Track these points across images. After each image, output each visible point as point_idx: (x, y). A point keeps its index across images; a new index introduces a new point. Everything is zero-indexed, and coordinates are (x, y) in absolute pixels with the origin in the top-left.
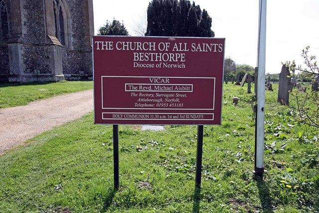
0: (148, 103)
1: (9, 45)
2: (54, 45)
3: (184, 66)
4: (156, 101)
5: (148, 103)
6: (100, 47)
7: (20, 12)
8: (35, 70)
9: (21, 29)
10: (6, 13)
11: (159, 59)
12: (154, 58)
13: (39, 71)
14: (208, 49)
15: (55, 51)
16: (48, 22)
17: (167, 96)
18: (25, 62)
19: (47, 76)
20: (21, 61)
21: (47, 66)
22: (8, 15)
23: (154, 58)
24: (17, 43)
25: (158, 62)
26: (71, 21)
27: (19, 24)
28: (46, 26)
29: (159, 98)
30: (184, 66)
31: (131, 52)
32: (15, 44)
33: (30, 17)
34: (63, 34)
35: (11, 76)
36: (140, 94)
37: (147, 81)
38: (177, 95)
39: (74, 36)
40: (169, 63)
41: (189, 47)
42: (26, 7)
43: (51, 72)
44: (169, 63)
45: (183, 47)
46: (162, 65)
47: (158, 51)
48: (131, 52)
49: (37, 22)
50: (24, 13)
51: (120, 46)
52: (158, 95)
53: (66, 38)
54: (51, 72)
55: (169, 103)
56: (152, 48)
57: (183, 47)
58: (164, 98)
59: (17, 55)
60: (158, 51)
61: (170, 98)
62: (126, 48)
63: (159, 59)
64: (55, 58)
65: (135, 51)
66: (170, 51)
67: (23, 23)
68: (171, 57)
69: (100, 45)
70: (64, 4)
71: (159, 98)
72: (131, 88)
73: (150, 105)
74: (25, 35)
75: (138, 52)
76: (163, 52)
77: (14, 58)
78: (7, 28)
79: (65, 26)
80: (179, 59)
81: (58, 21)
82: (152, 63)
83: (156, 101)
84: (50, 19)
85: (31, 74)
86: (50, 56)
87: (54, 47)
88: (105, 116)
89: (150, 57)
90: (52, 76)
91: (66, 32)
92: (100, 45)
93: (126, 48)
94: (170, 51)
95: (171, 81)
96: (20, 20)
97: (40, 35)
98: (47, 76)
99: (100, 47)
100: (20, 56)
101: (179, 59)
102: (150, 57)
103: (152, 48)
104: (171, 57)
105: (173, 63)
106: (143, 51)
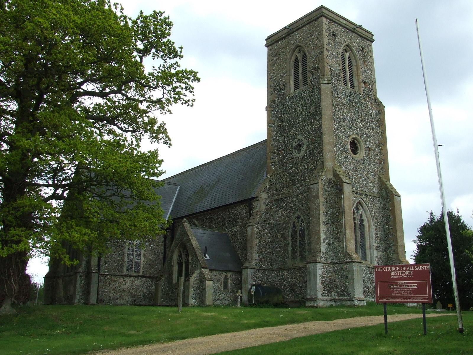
0: (398, 293)
1: (308, 265)
2: (354, 262)
3: (412, 276)
4: (401, 292)
5: (398, 293)
6: (377, 270)
7: (320, 230)
8: (333, 293)
9: (320, 247)
10: (304, 229)
11: (401, 274)
12: (399, 274)
13: (336, 294)
14: (422, 269)
15: (354, 268)
16: (347, 236)
17: (406, 290)
18: (323, 283)
19: (345, 300)
20: (319, 283)
21: (345, 288)
22: (307, 232)
23: (399, 274)
24: (316, 262)
25: (401, 275)
26: (373, 230)
27: (318, 242)
28: (346, 241)
29: (403, 291)
30: (412, 276)
31: (389, 272)
32: (314, 264)
33: (329, 234)
34: (363, 247)
35: (308, 300)
36: (394, 289)
37: (397, 283)
38: (411, 289)
39: (377, 248)
40: (406, 275)
41: (414, 268)
42: (325, 224)
43: (349, 295)
44: (406, 275)
45: (411, 269)
46: (403, 276)
47: (400, 270)
48: (389, 272)
49: (337, 237)
50: (323, 229)
51: (385, 269)
52: (402, 290)
53: (368, 252)
54: (349, 295)
55: (407, 293)
56: (398, 269)
57: (411, 269)
58: (405, 291)
59: (315, 275)
60: (400, 270)
61: (408, 291)
62: (387, 270)
63: (401, 274)
64: (355, 278)
65: (391, 271)
66: (406, 270)
67: (322, 240)
68: (406, 273)
69: (377, 269)
70: (365, 211)
71: (403, 291)
72: (390, 287)
73: (399, 294)
74: (323, 253)
75: (393, 271)
76: (403, 271)
77: (312, 279)
78: (300, 243)
79: (367, 237)
80: (410, 274)
81: (358, 232)
82: (398, 276)
83: (401, 292)
84: (349, 233)
85: (328, 298)
86: (350, 276)
87: (354, 264)
88: (380, 299)
89: (397, 273)
90: (351, 300)
91: (368, 244)
92: (377, 269)
93: (387, 270)
94: (406, 270)
95: (408, 283)
96: (319, 238)
97: (339, 252)
98: (345, 300)
99: (377, 270)
100: (318, 276)
101: (410, 274)
102: (397, 273)
103: (398, 269)
104: (406, 273)
105: (407, 275)
106: (395, 271)
